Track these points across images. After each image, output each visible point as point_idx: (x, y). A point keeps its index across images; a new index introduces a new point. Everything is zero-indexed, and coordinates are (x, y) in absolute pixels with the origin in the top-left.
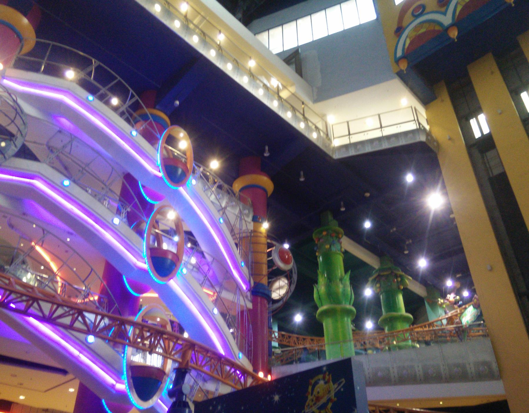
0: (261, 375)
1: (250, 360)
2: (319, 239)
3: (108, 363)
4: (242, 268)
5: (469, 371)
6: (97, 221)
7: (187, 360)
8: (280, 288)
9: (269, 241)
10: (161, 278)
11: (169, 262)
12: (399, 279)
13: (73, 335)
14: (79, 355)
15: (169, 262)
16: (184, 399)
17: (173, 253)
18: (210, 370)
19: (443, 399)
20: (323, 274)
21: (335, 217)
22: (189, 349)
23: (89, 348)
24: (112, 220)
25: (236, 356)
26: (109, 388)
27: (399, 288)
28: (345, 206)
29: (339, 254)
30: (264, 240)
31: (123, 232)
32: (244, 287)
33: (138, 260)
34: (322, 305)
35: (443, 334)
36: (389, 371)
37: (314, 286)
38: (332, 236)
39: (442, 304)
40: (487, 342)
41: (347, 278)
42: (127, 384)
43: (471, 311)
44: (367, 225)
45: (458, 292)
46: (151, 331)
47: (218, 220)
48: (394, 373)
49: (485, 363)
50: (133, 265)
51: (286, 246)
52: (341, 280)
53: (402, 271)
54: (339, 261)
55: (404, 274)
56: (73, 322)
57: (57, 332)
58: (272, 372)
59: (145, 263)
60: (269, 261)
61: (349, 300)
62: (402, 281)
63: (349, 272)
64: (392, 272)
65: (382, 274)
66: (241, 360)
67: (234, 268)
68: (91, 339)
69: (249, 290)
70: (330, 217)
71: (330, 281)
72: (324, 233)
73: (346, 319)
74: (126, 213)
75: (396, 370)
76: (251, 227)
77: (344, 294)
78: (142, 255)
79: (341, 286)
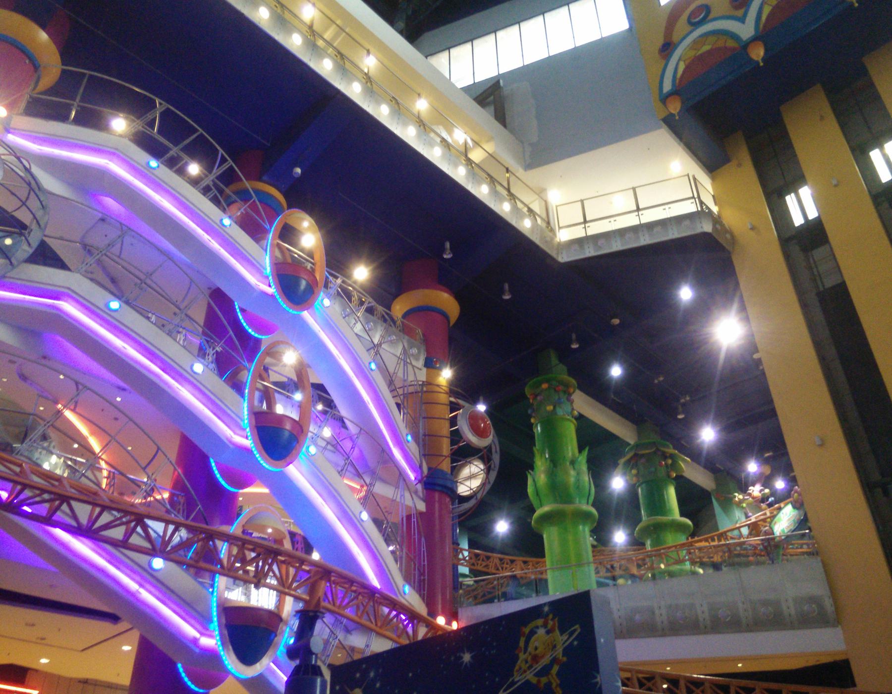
0: (441, 621)
1: (422, 597)
2: (536, 396)
4: (408, 444)
8: (471, 477)
12: (670, 461)
13: (128, 558)
16: (313, 662)
19: (740, 660)
20: (542, 453)
21: (561, 360)
27: (669, 476)
28: (578, 340)
29: (568, 420)
30: (444, 398)
34: (541, 506)
35: (742, 552)
36: (653, 613)
39: (741, 501)
42: (218, 638)
43: (788, 514)
44: (616, 371)
45: (767, 481)
46: (259, 550)
48: (662, 616)
49: (812, 599)
52: (573, 462)
53: (675, 448)
54: (569, 432)
56: (128, 534)
58: (460, 617)
59: (247, 438)
62: (674, 466)
64: (658, 450)
65: (640, 452)
68: (158, 563)
70: (554, 360)
72: (545, 386)
73: (581, 527)
77: (578, 487)
78: (242, 423)
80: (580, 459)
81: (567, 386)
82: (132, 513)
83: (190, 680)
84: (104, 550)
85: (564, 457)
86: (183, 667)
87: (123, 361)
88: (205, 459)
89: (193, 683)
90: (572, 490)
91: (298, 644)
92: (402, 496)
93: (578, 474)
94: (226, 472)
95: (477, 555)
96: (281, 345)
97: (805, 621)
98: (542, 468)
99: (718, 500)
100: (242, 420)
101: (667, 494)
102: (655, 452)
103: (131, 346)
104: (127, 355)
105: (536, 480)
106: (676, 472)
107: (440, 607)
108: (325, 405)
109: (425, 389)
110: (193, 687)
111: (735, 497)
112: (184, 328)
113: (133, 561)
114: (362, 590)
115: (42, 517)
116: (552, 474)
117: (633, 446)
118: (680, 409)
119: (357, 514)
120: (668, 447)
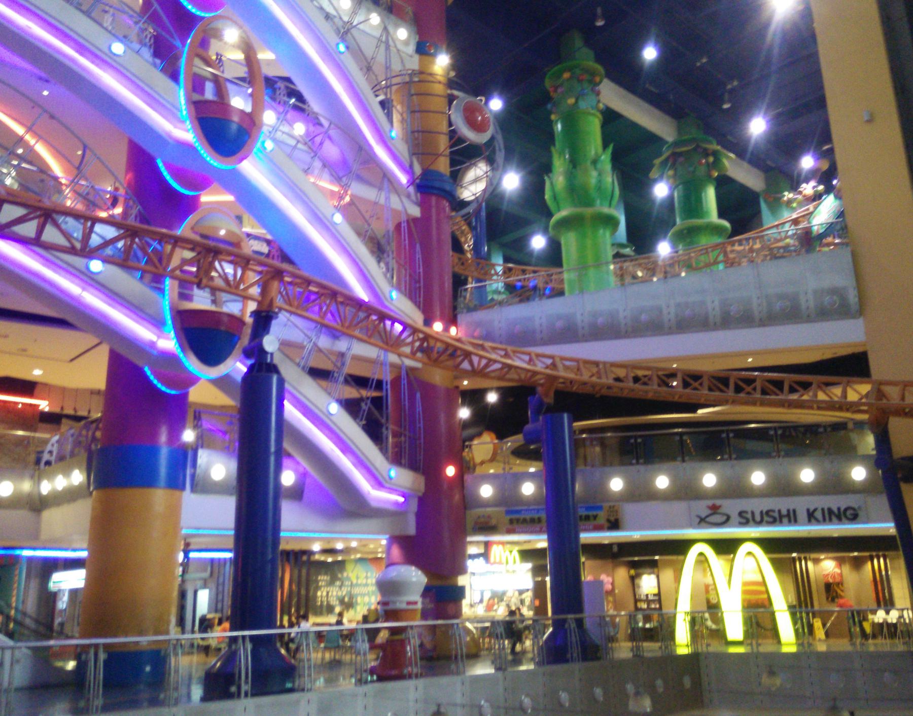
0: (438, 327)
1: (417, 304)
2: (556, 88)
3: (137, 307)
4: (393, 142)
5: (803, 306)
6: (81, 49)
7: (270, 298)
8: (476, 180)
9: (449, 92)
10: (221, 158)
11: (234, 127)
12: (711, 159)
13: (61, 260)
14: (80, 295)
15: (234, 127)
16: (269, 360)
17: (242, 112)
18: (319, 315)
20: (562, 153)
21: (588, 43)
22: (273, 278)
23: (93, 279)
24: (109, 48)
25: (385, 296)
26: (147, 348)
27: (710, 176)
28: (605, 16)
29: (593, 115)
30: (440, 89)
31: (134, 70)
32: (403, 179)
33: (175, 127)
34: (559, 210)
36: (661, 312)
37: (546, 178)
38: (580, 81)
39: (790, 202)
40: (846, 254)
41: (606, 159)
44: (650, 53)
46: (198, 249)
47: (334, 46)
48: (670, 314)
49: (834, 291)
50: (167, 138)
51: (496, 104)
52: (595, 162)
53: (718, 144)
54: (594, 127)
55: (719, 148)
56: (40, 231)
57: (32, 254)
59: (187, 131)
60: (451, 131)
61: (609, 198)
62: (717, 163)
63: (611, 147)
64: (698, 146)
65: (678, 150)
66: (395, 303)
67: (377, 142)
68: (96, 266)
69: (411, 182)
70: (578, 42)
71: (574, 167)
72: (566, 75)
73: (601, 231)
74: (150, 38)
75: (673, 310)
76: (414, 63)
77: (599, 188)
78: (179, 114)
79: (594, 174)
80: (603, 157)
81: (593, 74)
82: (39, 209)
83: (159, 381)
84: (34, 251)
85: (585, 155)
86: (150, 369)
87: (38, 49)
88: (151, 161)
89: (163, 384)
90: (593, 193)
91: (252, 344)
92: (387, 199)
93: (600, 175)
94: (177, 173)
95: (510, 269)
96: (229, 23)
97: (823, 314)
98: (561, 170)
99: (766, 201)
100: (179, 110)
101: (705, 195)
102: (695, 149)
103: (36, 24)
104: (32, 36)
105: (554, 183)
106: (719, 171)
107: (438, 313)
108: (297, 100)
109: (416, 79)
110: (163, 389)
111: (784, 196)
112: (111, 7)
113: (66, 263)
114: (322, 291)
115: (32, 239)
116: (570, 176)
117: (672, 144)
118: (726, 96)
119: (329, 216)
120: (710, 142)
